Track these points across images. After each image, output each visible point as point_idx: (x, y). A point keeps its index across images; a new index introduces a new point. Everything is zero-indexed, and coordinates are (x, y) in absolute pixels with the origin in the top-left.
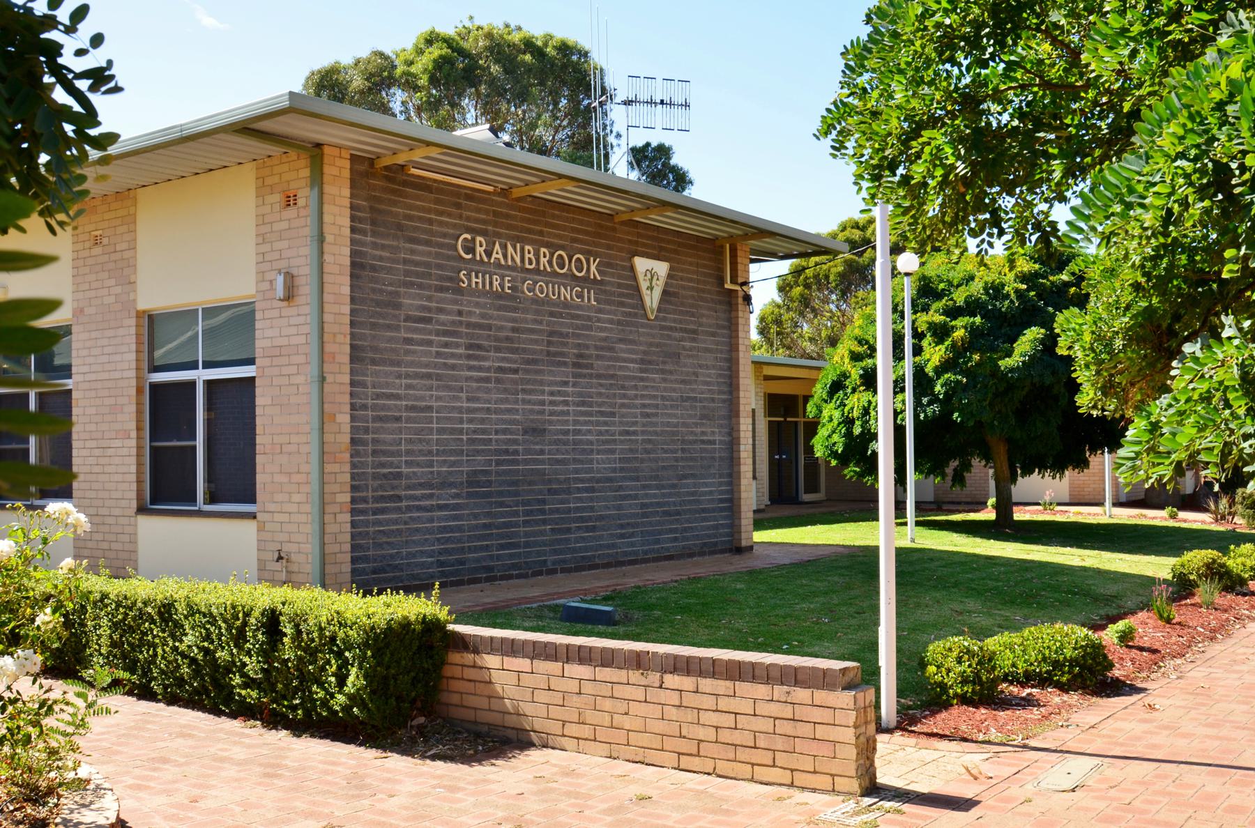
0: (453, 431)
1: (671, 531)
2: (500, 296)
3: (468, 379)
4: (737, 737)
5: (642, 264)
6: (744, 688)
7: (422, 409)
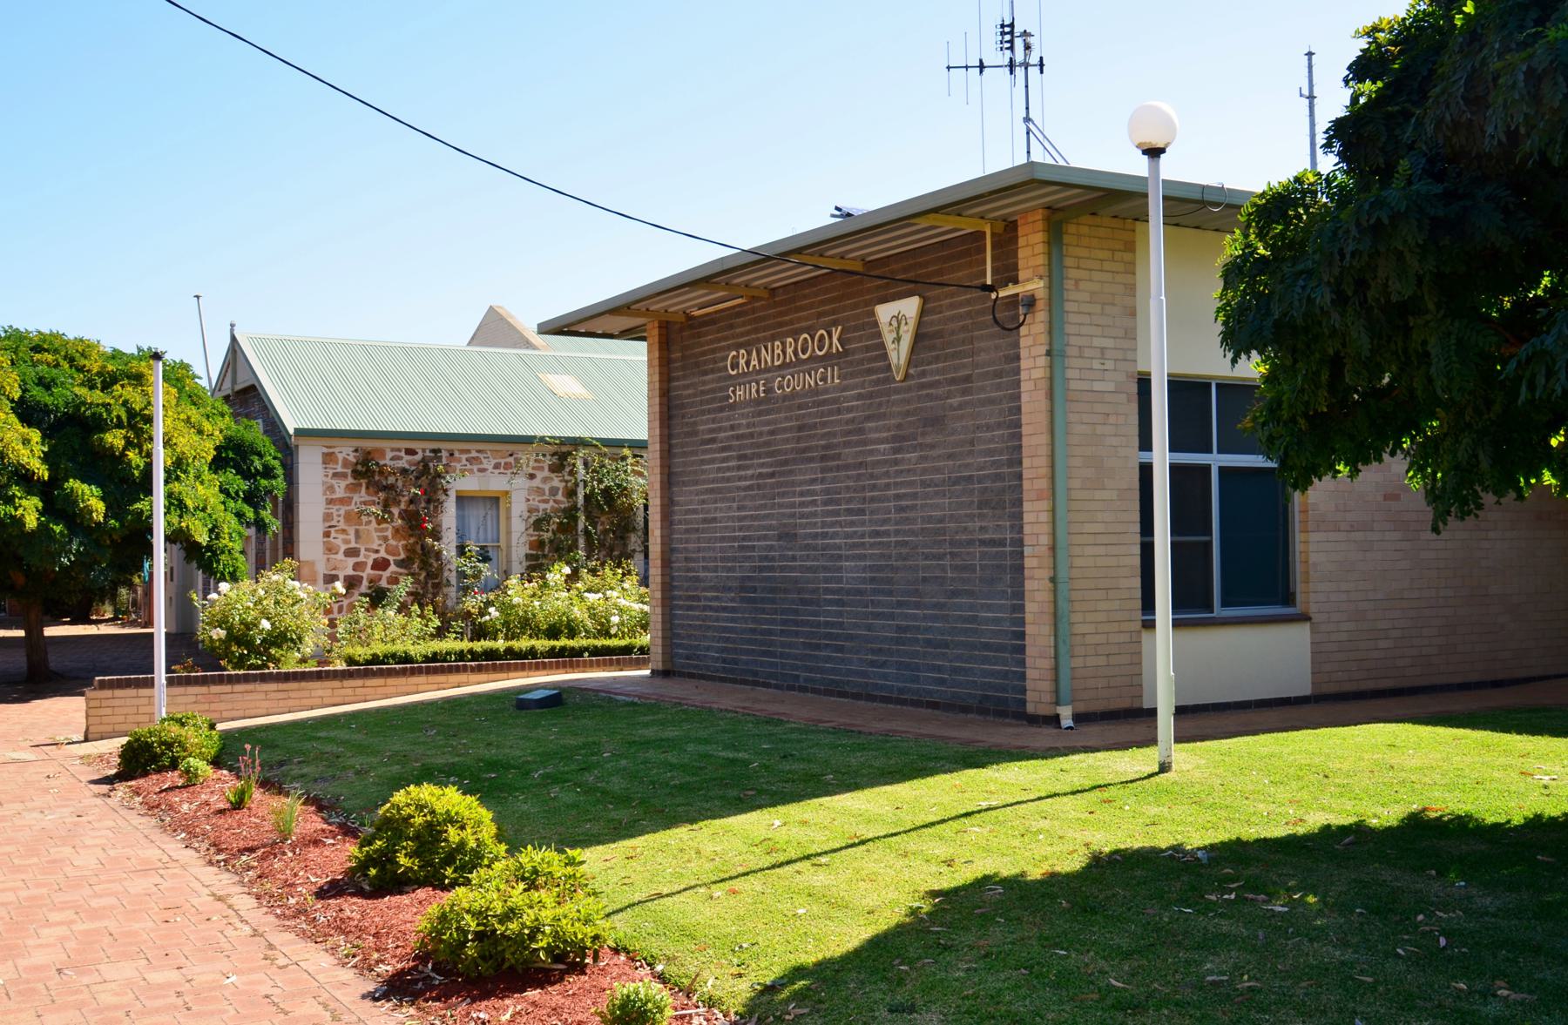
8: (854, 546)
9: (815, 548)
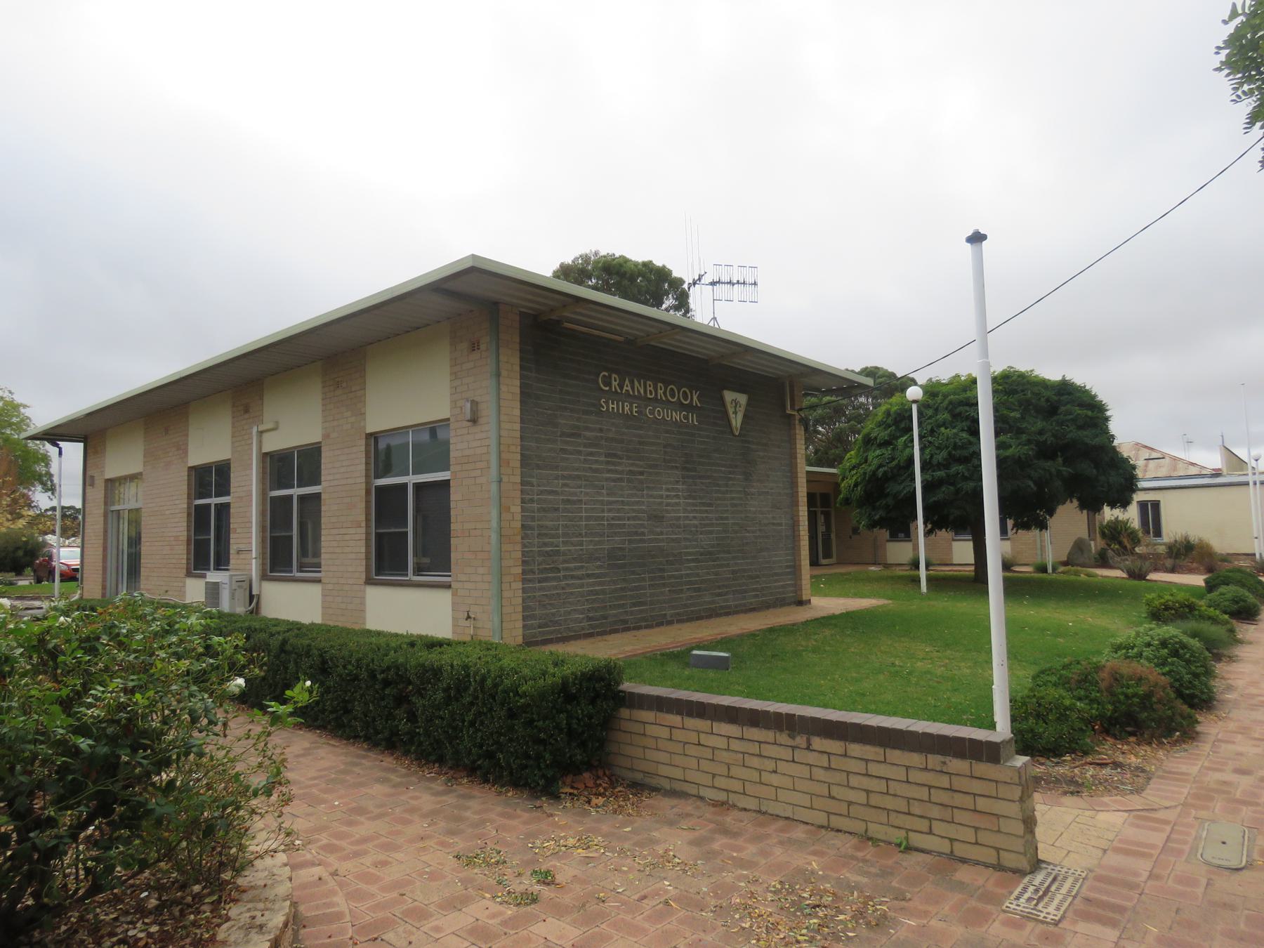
0: (597, 519)
1: (754, 590)
2: (629, 417)
3: (607, 479)
4: (889, 803)
5: (729, 396)
6: (895, 755)
7: (574, 502)
8: (706, 525)
9: (679, 527)
